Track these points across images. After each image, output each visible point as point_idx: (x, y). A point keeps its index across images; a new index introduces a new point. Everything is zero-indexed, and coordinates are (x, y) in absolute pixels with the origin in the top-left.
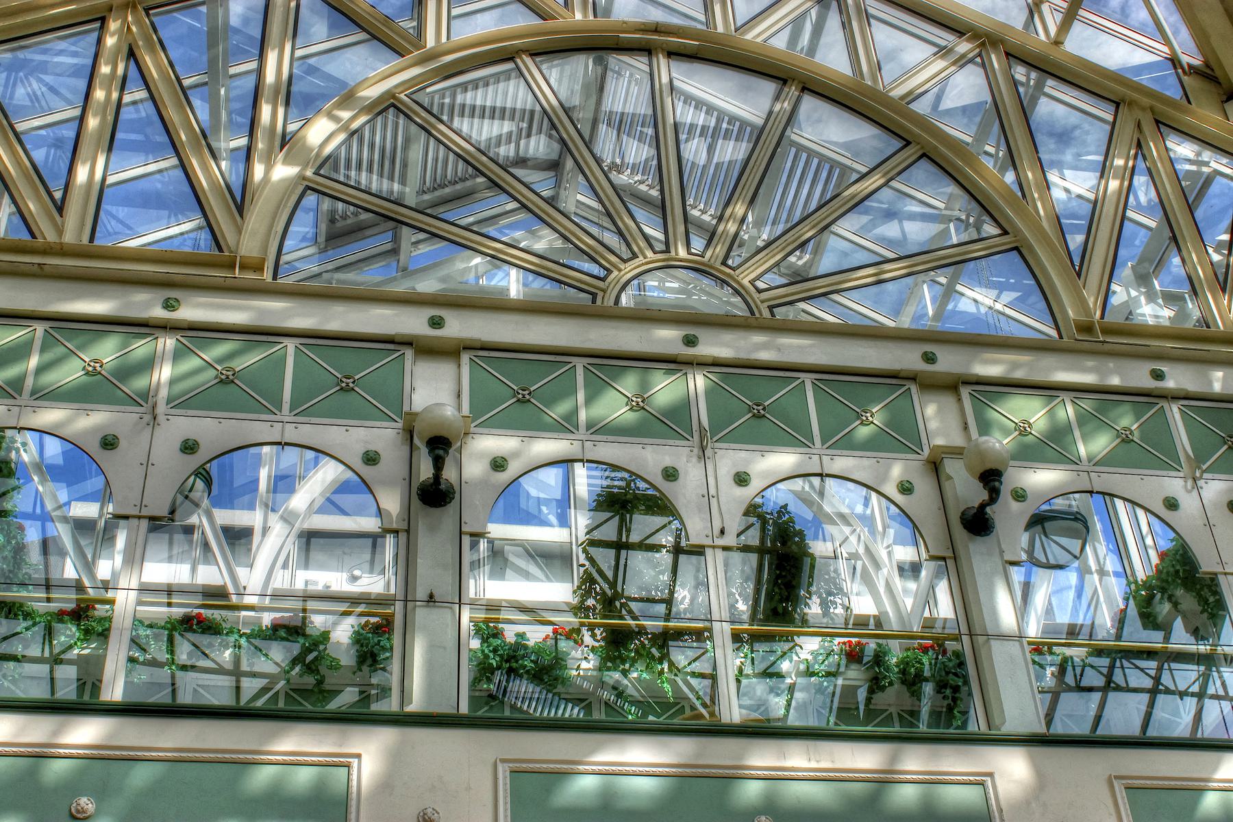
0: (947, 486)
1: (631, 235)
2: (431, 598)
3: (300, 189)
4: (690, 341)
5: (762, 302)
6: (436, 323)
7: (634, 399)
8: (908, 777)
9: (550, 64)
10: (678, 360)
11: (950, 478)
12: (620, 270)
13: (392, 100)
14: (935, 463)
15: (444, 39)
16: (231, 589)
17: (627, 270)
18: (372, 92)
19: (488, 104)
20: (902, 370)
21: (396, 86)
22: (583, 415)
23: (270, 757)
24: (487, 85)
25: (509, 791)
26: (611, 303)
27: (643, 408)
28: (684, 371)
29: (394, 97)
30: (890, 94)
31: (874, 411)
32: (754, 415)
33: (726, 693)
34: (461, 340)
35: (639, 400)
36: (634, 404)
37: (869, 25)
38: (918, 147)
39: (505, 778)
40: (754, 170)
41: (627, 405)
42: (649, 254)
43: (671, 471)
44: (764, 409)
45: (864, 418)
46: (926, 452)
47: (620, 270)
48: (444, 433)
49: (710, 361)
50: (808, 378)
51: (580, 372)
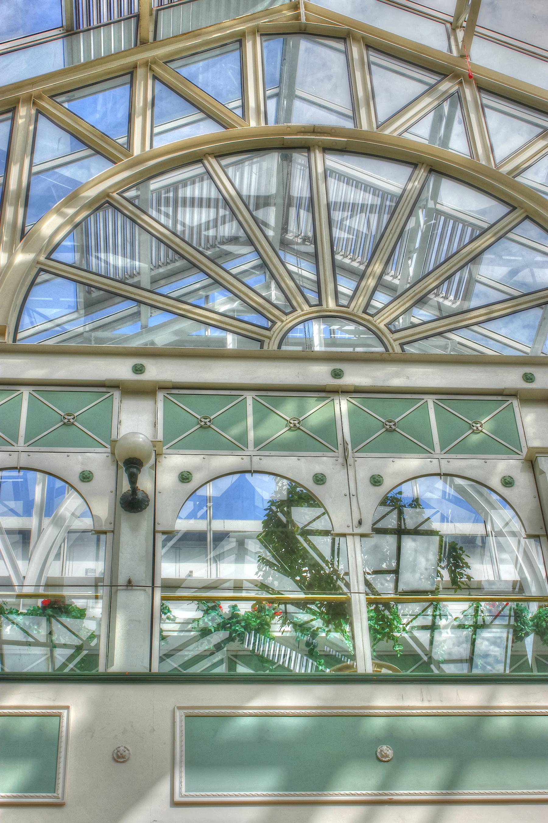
0: (540, 478)
1: (292, 293)
2: (130, 584)
3: (35, 271)
4: (337, 374)
5: (395, 340)
6: (138, 369)
7: (292, 421)
8: (502, 711)
9: (251, 161)
10: (326, 390)
11: (542, 472)
12: (282, 321)
13: (107, 199)
14: (532, 461)
15: (147, 148)
16: (15, 582)
17: (288, 321)
18: (92, 193)
19: (205, 195)
20: (505, 389)
21: (110, 187)
22: (251, 435)
23: (376, 711)
24: (194, 183)
25: (184, 732)
26: (275, 347)
27: (299, 428)
28: (332, 398)
29: (108, 195)
30: (500, 171)
31: (483, 422)
32: (387, 430)
33: (362, 649)
34: (157, 382)
35: (296, 422)
36: (292, 425)
37: (485, 116)
38: (522, 211)
39: (181, 721)
40: (390, 237)
41: (286, 426)
42: (306, 308)
43: (320, 477)
44: (395, 425)
45: (475, 428)
46: (525, 450)
47: (282, 321)
48: (137, 455)
49: (352, 389)
50: (430, 401)
51: (431, 405)
